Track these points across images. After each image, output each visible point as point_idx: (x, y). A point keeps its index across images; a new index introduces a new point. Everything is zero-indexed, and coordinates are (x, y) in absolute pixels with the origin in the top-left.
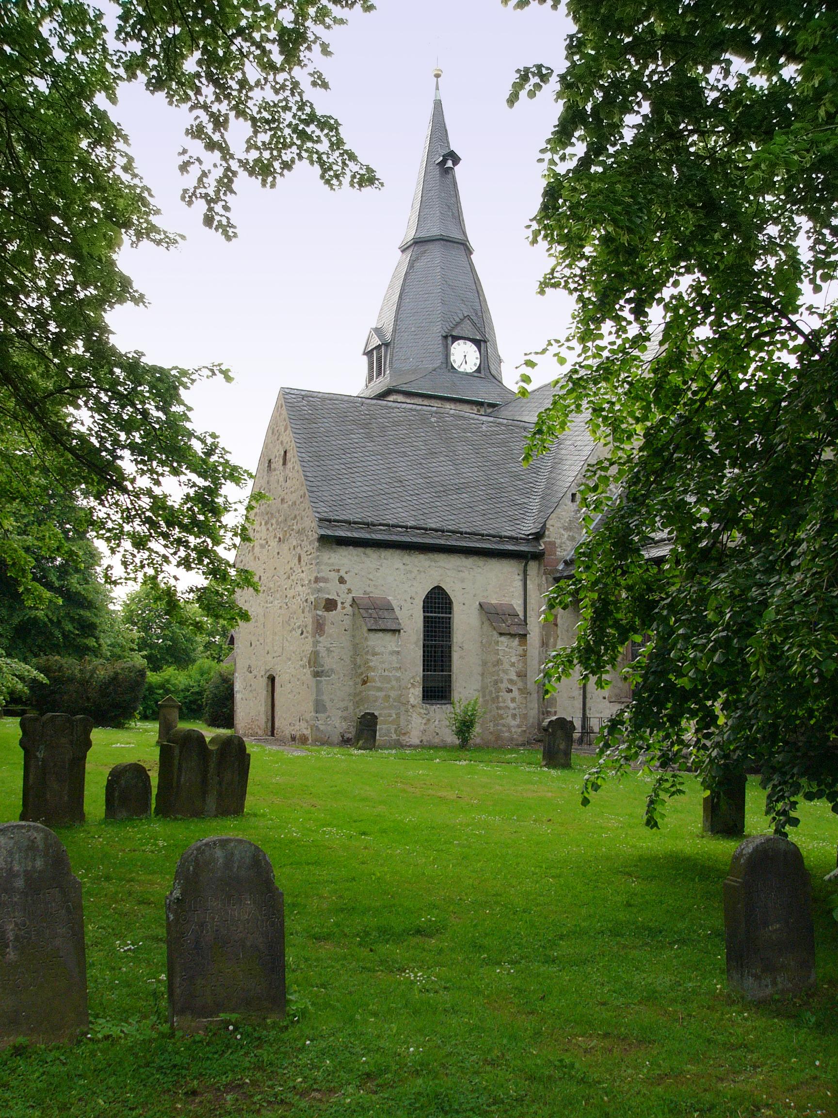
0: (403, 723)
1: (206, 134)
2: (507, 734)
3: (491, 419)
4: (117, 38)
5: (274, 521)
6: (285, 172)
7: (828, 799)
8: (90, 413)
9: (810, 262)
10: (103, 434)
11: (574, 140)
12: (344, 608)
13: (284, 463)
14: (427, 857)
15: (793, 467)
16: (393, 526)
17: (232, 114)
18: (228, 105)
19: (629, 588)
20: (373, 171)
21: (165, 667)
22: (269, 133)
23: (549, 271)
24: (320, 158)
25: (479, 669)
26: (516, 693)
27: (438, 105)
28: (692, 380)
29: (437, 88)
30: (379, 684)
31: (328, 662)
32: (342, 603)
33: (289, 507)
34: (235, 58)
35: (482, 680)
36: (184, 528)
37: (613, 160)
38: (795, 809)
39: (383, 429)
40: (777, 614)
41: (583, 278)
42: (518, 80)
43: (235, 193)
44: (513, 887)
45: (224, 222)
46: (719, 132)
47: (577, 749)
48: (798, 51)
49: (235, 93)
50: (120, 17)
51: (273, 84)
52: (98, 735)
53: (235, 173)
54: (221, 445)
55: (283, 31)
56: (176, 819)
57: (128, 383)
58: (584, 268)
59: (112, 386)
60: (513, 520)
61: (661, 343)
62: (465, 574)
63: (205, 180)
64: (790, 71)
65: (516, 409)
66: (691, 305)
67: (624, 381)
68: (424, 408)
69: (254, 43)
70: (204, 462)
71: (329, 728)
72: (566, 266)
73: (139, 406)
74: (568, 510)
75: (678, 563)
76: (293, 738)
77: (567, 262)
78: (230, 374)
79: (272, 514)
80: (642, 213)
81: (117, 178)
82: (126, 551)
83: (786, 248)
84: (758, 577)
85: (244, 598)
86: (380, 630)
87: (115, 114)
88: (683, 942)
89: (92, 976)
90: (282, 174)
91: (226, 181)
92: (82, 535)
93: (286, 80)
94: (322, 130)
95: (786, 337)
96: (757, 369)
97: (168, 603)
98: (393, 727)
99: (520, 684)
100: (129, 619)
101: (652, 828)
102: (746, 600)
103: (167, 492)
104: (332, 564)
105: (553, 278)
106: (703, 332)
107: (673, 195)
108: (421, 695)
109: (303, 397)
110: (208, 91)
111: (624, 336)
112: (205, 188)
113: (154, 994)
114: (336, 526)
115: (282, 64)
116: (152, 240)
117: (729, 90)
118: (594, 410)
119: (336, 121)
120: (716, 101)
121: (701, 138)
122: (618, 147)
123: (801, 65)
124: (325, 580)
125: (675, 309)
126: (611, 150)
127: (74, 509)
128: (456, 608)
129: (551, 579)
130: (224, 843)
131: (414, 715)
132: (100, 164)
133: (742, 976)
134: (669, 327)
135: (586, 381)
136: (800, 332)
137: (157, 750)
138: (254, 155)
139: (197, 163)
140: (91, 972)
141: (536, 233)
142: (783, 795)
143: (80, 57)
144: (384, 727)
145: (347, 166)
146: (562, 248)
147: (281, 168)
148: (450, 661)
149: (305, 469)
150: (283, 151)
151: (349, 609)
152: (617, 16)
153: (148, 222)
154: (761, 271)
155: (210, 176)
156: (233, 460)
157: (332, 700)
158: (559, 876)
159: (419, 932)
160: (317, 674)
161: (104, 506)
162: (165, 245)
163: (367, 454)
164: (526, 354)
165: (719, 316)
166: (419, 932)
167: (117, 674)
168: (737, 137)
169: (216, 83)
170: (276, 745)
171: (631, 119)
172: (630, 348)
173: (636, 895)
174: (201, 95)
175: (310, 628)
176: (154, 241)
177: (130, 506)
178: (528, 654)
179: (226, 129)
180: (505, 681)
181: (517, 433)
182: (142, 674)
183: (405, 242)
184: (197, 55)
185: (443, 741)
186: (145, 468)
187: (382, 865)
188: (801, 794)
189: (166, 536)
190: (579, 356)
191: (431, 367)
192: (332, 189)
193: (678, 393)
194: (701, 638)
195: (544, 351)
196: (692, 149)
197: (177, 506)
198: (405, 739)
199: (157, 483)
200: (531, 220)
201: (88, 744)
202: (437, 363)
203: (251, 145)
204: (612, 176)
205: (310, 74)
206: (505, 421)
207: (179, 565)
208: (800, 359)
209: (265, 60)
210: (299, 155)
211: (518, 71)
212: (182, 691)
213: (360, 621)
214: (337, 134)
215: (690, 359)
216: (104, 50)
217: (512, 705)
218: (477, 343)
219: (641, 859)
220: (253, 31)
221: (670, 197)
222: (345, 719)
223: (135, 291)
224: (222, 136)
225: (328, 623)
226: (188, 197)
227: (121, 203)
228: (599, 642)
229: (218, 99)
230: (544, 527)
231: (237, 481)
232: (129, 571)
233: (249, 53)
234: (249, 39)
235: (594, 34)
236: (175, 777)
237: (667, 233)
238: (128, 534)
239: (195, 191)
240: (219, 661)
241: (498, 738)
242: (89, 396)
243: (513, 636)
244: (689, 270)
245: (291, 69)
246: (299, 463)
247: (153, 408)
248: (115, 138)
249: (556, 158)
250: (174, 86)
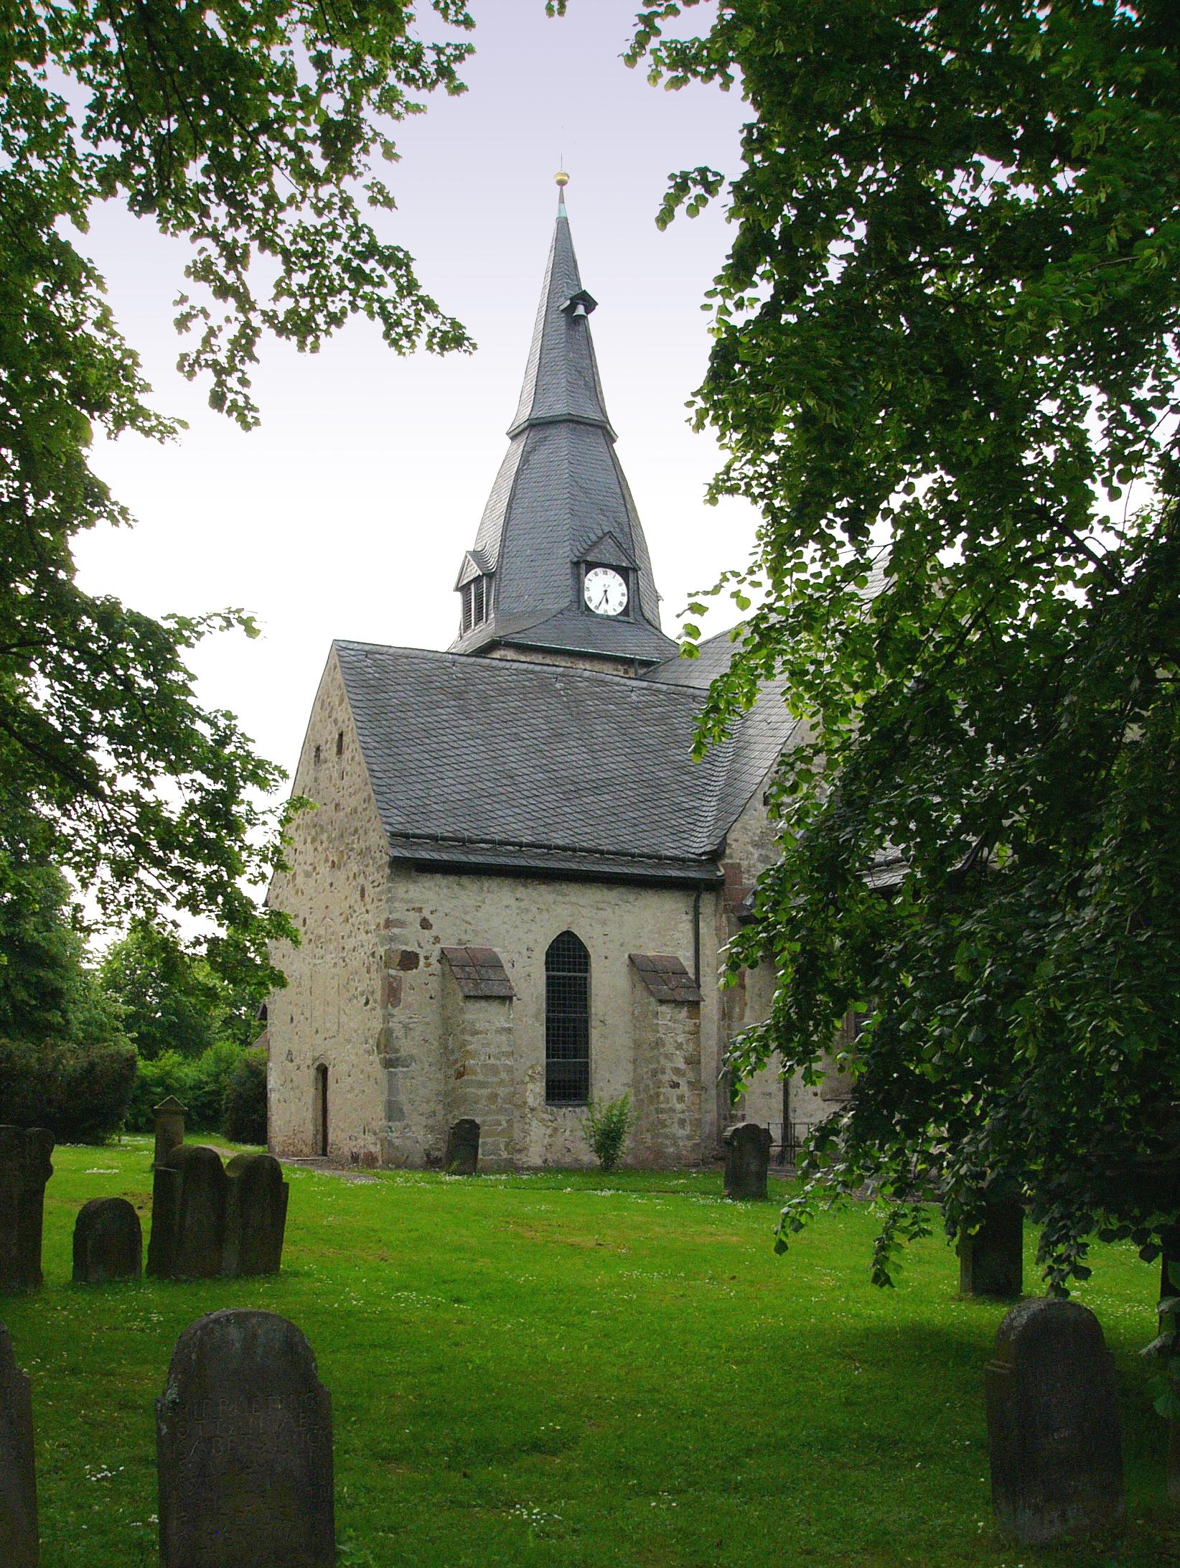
0: (517, 1134)
1: (216, 273)
2: (672, 1150)
3: (645, 684)
4: (85, 136)
5: (324, 837)
6: (333, 328)
7: (1133, 1239)
8: (47, 681)
9: (1103, 453)
10: (68, 713)
11: (755, 278)
12: (428, 965)
13: (340, 751)
14: (552, 1334)
15: (1083, 753)
16: (502, 843)
17: (254, 245)
18: (249, 231)
19: (846, 934)
20: (461, 327)
21: (161, 1053)
22: (309, 272)
23: (722, 469)
24: (383, 308)
25: (630, 1054)
26: (684, 1088)
27: (563, 227)
28: (935, 627)
29: (562, 200)
30: (481, 1078)
31: (406, 1046)
32: (426, 958)
33: (346, 816)
34: (258, 164)
35: (635, 1070)
36: (186, 851)
37: (812, 305)
38: (1085, 1253)
39: (484, 699)
40: (1057, 968)
41: (771, 478)
42: (672, 191)
43: (257, 361)
44: (678, 1377)
45: (241, 402)
46: (966, 265)
47: (776, 1171)
48: (1074, 154)
49: (258, 215)
50: (91, 107)
51: (314, 201)
52: (63, 1157)
53: (256, 332)
54: (239, 730)
55: (327, 124)
56: (178, 1281)
57: (103, 637)
58: (773, 463)
59: (80, 642)
60: (677, 833)
61: (888, 573)
62: (608, 914)
63: (213, 340)
64: (1065, 180)
65: (682, 669)
66: (931, 516)
67: (835, 630)
68: (545, 668)
69: (284, 141)
70: (216, 755)
71: (408, 1143)
72: (748, 462)
73: (120, 672)
74: (758, 816)
75: (916, 895)
76: (355, 1158)
77: (749, 456)
78: (254, 624)
79: (322, 827)
80: (857, 380)
81: (88, 339)
82: (103, 882)
83: (1069, 431)
84: (1031, 914)
85: (280, 953)
87: (82, 245)
88: (927, 1458)
89: (48, 1519)
90: (327, 333)
91: (243, 341)
92: (42, 860)
93: (332, 195)
94: (386, 268)
95: (1071, 562)
96: (1031, 609)
97: (165, 962)
98: (502, 1142)
99: (691, 1076)
100: (113, 982)
101: (882, 1286)
102: (1015, 949)
103: (162, 798)
104: (411, 901)
105: (729, 479)
106: (951, 556)
107: (900, 355)
108: (544, 1093)
109: (367, 654)
110: (219, 212)
111: (833, 564)
112: (213, 352)
113: (140, 1545)
115: (326, 173)
116: (139, 428)
117: (979, 206)
118: (792, 674)
119: (406, 254)
120: (962, 220)
121: (940, 275)
122: (820, 288)
123: (1083, 171)
124: (401, 924)
125: (908, 524)
126: (810, 292)
127: (28, 820)
129: (734, 919)
130: (242, 1318)
131: (535, 1123)
132: (61, 319)
133: (1015, 1510)
134: (898, 548)
135: (780, 631)
136: (1091, 556)
137: (151, 1178)
138: (286, 303)
139: (201, 316)
140: (47, 1513)
141: (702, 414)
142: (1066, 1234)
143: (36, 164)
144: (489, 1140)
145: (423, 319)
146: (739, 436)
147: (326, 323)
148: (587, 1043)
149: (370, 760)
150: (330, 299)
151: (436, 967)
152: (817, 98)
153: (132, 402)
154: (1033, 468)
155: (220, 335)
156: (258, 751)
157: (412, 1101)
158: (746, 1361)
159: (536, 1446)
160: (388, 1064)
161: (70, 818)
162: (158, 435)
163: (461, 737)
164: (690, 595)
165: (973, 534)
166: (536, 1446)
167: (92, 1065)
168: (992, 272)
169: (231, 201)
170: (329, 1168)
171: (838, 248)
172: (842, 581)
173: (860, 1387)
174: (209, 217)
175: (378, 995)
176: (142, 429)
177: (108, 819)
178: (703, 1030)
179: (245, 268)
180: (668, 1071)
181: (683, 704)
182: (130, 1063)
183: (517, 424)
184: (204, 160)
185: (577, 1160)
186: (130, 763)
187: (482, 1347)
188: (1094, 1232)
189: (159, 863)
190: (768, 594)
191: (557, 607)
192: (400, 353)
193: (913, 646)
194: (949, 1007)
195: (717, 590)
196: (929, 291)
197: (175, 818)
198: (521, 1159)
199: (148, 784)
200: (694, 394)
201: (48, 1171)
202: (565, 603)
203: (281, 290)
204: (810, 329)
205: (367, 187)
206: (665, 687)
207: (178, 906)
208: (1091, 595)
209: (303, 166)
210: (352, 304)
211: (672, 177)
212: (191, 1088)
213: (453, 985)
214: (409, 273)
215: (931, 597)
216: (71, 151)
217: (679, 1107)
218: (624, 572)
219: (868, 1333)
220: (284, 126)
221: (896, 358)
222: (431, 1129)
223: (113, 504)
224: (239, 278)
225: (405, 986)
226: (188, 366)
227: (93, 375)
228: (804, 1016)
229: (233, 223)
230: (723, 843)
231: (262, 784)
232: (108, 911)
233: (279, 157)
234: (279, 137)
235: (782, 123)
236: (177, 1217)
237: (893, 412)
238: (106, 857)
239: (198, 357)
240: (245, 1043)
241: (659, 1153)
242: (46, 657)
243: (678, 1003)
244: (928, 469)
245: (339, 180)
246: (360, 750)
247: (139, 674)
248: (84, 281)
249: (730, 304)
250: (169, 204)
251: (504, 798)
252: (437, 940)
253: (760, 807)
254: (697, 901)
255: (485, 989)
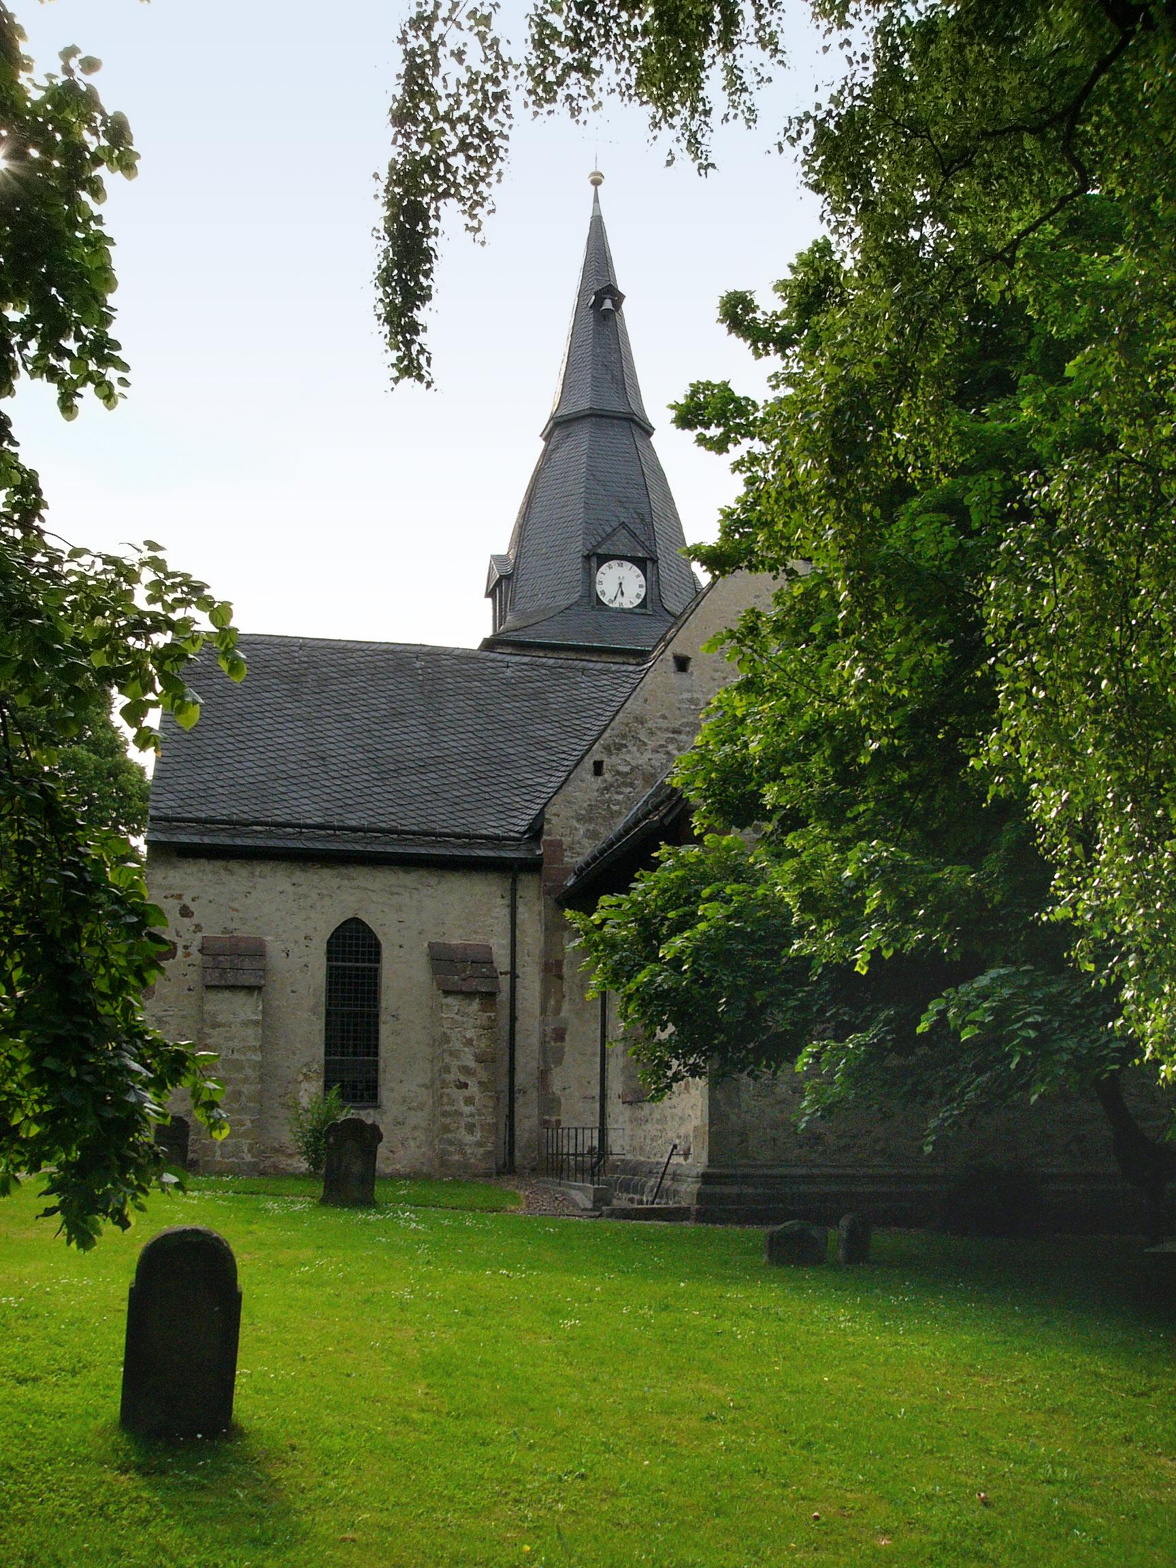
2: (457, 1157)
26: (473, 1089)
32: (186, 947)
86: (243, 987)
114: (178, 827)
128: (385, 954)
151: (196, 957)
180: (454, 1070)
191: (565, 603)
217: (467, 1110)
218: (640, 563)
243: (469, 995)
251: (305, 779)
252: (198, 928)
253: (589, 777)
254: (514, 882)
255: (231, 979)
